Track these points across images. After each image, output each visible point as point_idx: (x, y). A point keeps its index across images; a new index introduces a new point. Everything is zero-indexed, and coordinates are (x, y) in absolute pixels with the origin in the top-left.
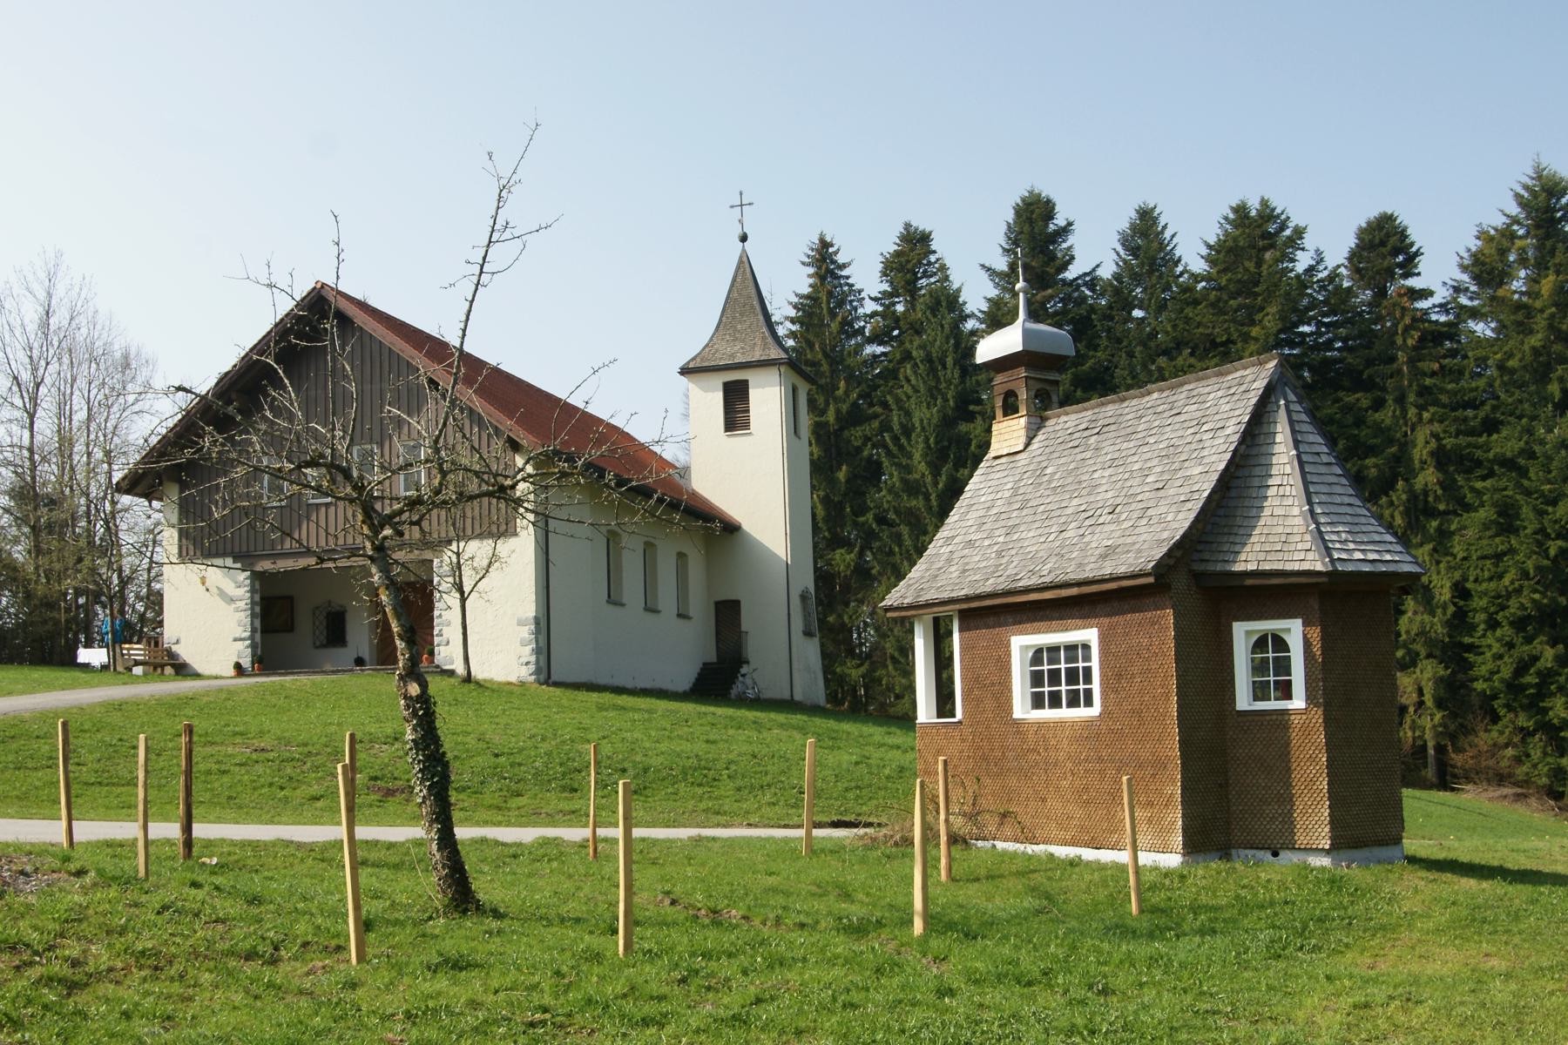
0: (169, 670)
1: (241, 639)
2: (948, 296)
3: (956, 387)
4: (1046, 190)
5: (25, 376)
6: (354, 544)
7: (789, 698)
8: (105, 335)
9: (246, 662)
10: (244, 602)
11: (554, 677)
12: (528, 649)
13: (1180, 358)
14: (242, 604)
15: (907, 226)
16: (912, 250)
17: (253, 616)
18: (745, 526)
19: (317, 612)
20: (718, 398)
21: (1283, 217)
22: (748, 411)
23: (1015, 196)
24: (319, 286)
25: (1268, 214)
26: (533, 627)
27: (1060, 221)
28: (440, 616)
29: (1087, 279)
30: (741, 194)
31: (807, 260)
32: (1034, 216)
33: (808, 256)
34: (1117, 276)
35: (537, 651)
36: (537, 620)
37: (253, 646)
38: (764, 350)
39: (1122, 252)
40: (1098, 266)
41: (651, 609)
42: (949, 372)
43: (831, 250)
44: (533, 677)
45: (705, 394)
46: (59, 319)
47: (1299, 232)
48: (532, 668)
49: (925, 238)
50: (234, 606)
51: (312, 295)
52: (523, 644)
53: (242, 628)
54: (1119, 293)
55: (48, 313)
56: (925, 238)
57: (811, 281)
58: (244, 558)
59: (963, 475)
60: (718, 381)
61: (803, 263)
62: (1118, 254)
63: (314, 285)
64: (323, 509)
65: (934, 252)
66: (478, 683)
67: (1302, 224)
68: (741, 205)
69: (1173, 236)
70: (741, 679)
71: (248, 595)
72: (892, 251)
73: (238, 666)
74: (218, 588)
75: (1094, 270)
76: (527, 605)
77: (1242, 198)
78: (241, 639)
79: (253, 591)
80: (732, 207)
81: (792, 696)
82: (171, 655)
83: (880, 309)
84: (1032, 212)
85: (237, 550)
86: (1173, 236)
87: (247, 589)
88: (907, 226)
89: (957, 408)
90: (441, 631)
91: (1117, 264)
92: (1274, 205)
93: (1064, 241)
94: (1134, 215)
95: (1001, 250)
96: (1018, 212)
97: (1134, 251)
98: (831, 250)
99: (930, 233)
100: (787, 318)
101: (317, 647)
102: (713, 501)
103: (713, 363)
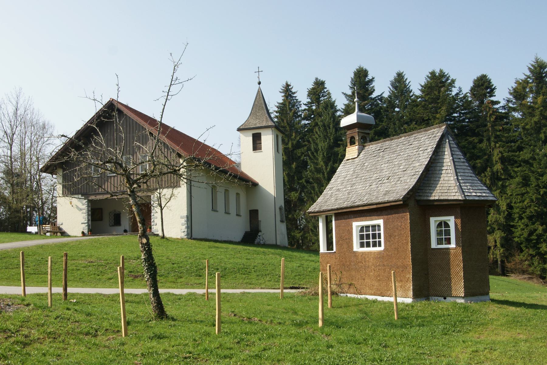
0: (59, 234)
1: (84, 223)
2: (331, 103)
3: (334, 135)
4: (365, 66)
5: (9, 131)
6: (123, 190)
8: (37, 117)
9: (86, 231)
10: (85, 210)
11: (193, 237)
12: (184, 227)
13: (412, 125)
14: (84, 211)
15: (317, 79)
16: (318, 87)
17: (88, 215)
18: (260, 184)
19: (111, 214)
20: (250, 139)
21: (448, 76)
22: (261, 144)
23: (354, 68)
24: (111, 100)
25: (442, 75)
26: (186, 219)
27: (370, 77)
28: (154, 215)
29: (379, 97)
30: (259, 68)
31: (281, 91)
32: (361, 75)
33: (282, 90)
34: (390, 97)
35: (187, 227)
36: (187, 217)
37: (88, 226)
38: (266, 122)
39: (391, 88)
40: (383, 93)
41: (227, 213)
42: (331, 130)
43: (290, 87)
44: (186, 237)
45: (246, 138)
46: (21, 111)
47: (453, 81)
48: (186, 233)
49: (323, 83)
50: (81, 212)
51: (109, 103)
52: (183, 225)
53: (84, 219)
54: (390, 102)
55: (17, 109)
56: (323, 83)
57: (283, 98)
58: (85, 195)
59: (336, 166)
60: (250, 133)
61: (280, 92)
62: (390, 89)
63: (109, 100)
64: (113, 178)
65: (326, 88)
66: (167, 239)
67: (454, 78)
68: (259, 72)
69: (409, 82)
70: (258, 237)
71: (87, 208)
72: (311, 88)
73: (83, 233)
74: (76, 205)
75: (382, 94)
76: (184, 211)
77: (433, 69)
78: (84, 223)
79: (88, 206)
80: (255, 72)
81: (276, 243)
82: (60, 229)
83: (307, 108)
84: (360, 74)
85: (83, 192)
86: (409, 82)
87: (86, 206)
88: (317, 79)
89: (334, 142)
90: (154, 220)
91: (390, 92)
92: (444, 72)
93: (371, 84)
94: (396, 75)
95: (349, 87)
96: (355, 74)
97: (395, 88)
98: (290, 87)
99: (325, 81)
100: (274, 111)
101: (111, 226)
102: (249, 175)
103: (249, 127)
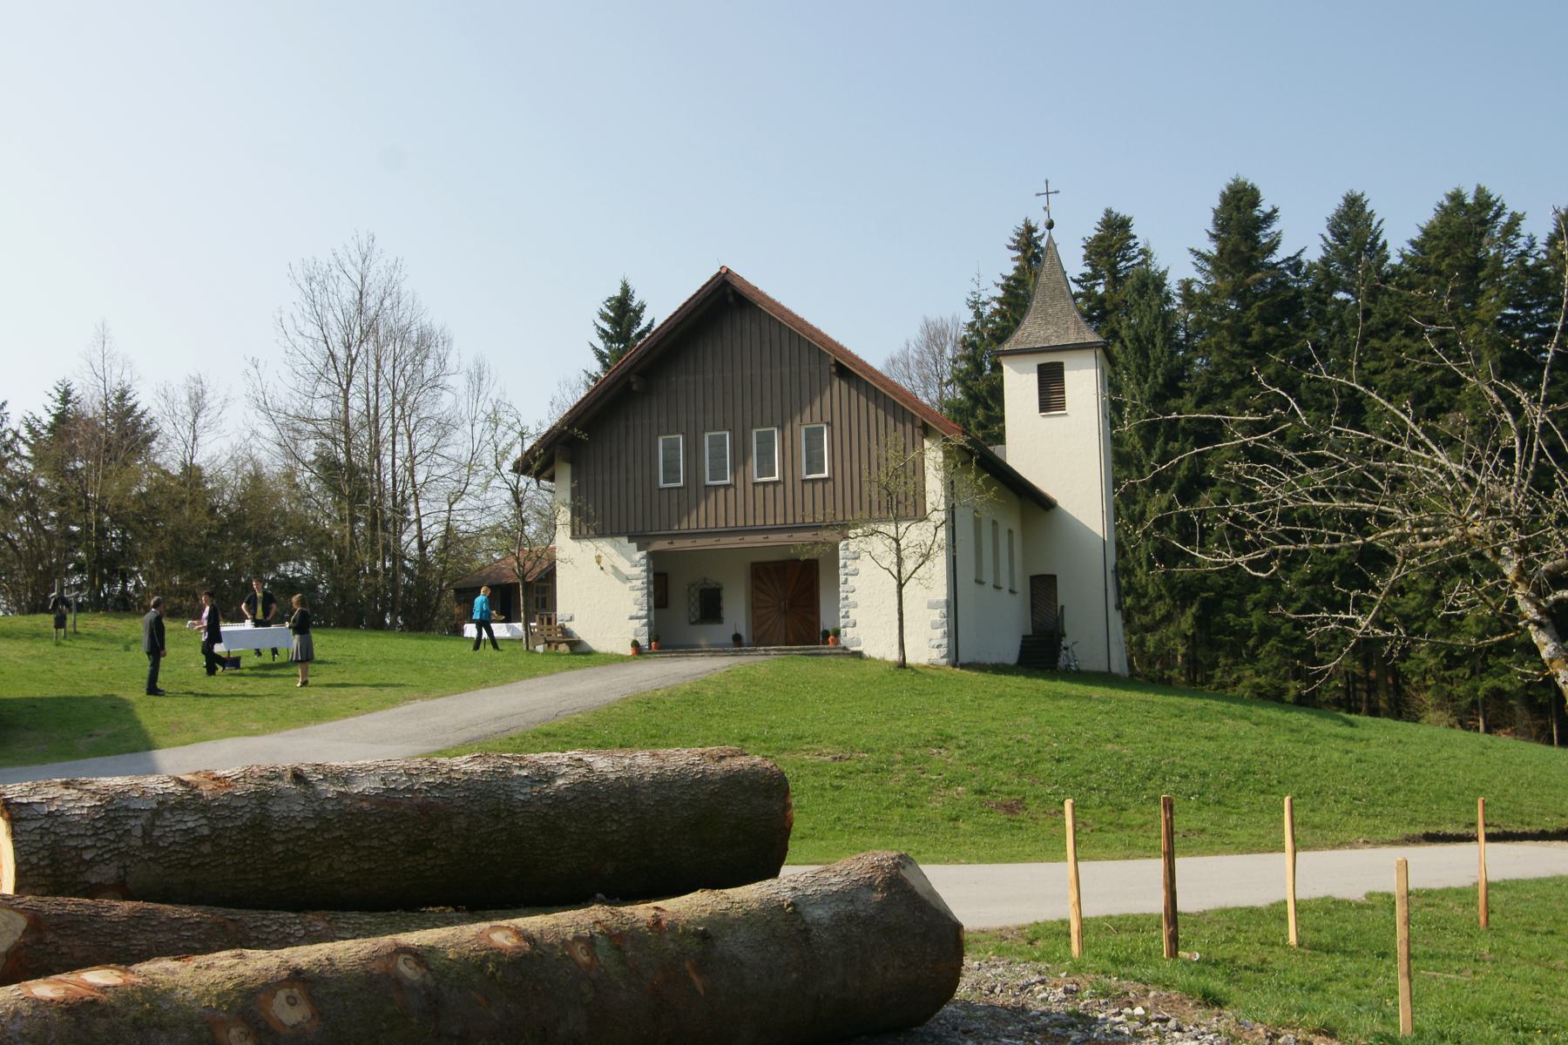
0: (563, 648)
1: (637, 618)
2: (1154, 279)
3: (1165, 364)
4: (1252, 178)
5: (341, 353)
6: (736, 526)
7: (893, 656)
8: (408, 314)
9: (643, 641)
10: (641, 581)
11: (963, 659)
12: (939, 632)
13: (1393, 339)
14: (638, 583)
15: (1108, 212)
16: (1113, 235)
17: (649, 594)
18: (1062, 503)
19: (693, 590)
20: (1033, 379)
21: (1499, 204)
22: (1063, 393)
23: (1221, 184)
24: (724, 271)
25: (1484, 201)
26: (944, 610)
27: (1265, 207)
28: (847, 598)
29: (1291, 262)
30: (1047, 182)
31: (1012, 244)
32: (1242, 203)
33: (1014, 241)
34: (1325, 262)
35: (948, 634)
36: (947, 602)
37: (649, 624)
38: (1078, 333)
39: (1330, 238)
40: (1302, 251)
41: (997, 587)
42: (1158, 350)
43: (1035, 235)
44: (945, 660)
45: (1019, 375)
46: (371, 302)
47: (1515, 220)
48: (944, 650)
49: (1124, 224)
50: (629, 585)
51: (716, 280)
52: (934, 626)
53: (638, 607)
54: (1326, 278)
55: (361, 293)
56: (1124, 224)
57: (1017, 264)
58: (639, 537)
59: (1173, 448)
60: (1033, 363)
61: (1009, 247)
62: (1325, 239)
63: (718, 270)
64: (722, 491)
65: (1135, 237)
66: (912, 668)
67: (1519, 212)
68: (1047, 193)
69: (1380, 223)
70: (1064, 652)
71: (645, 574)
72: (1092, 236)
73: (635, 644)
74: (613, 566)
75: (1298, 254)
76: (941, 592)
77: (1457, 186)
78: (637, 618)
79: (648, 571)
80: (1038, 195)
81: (1109, 668)
82: (566, 632)
83: (1082, 291)
84: (1241, 199)
85: (632, 529)
86: (1380, 223)
87: (642, 568)
88: (1108, 212)
89: (1165, 385)
90: (847, 612)
91: (1324, 249)
92: (1491, 192)
93: (1269, 227)
94: (1342, 202)
95: (1207, 236)
96: (1226, 200)
97: (1340, 235)
98: (1035, 235)
99: (1130, 220)
100: (994, 299)
101: (693, 623)
102: (1028, 479)
103: (1028, 346)
